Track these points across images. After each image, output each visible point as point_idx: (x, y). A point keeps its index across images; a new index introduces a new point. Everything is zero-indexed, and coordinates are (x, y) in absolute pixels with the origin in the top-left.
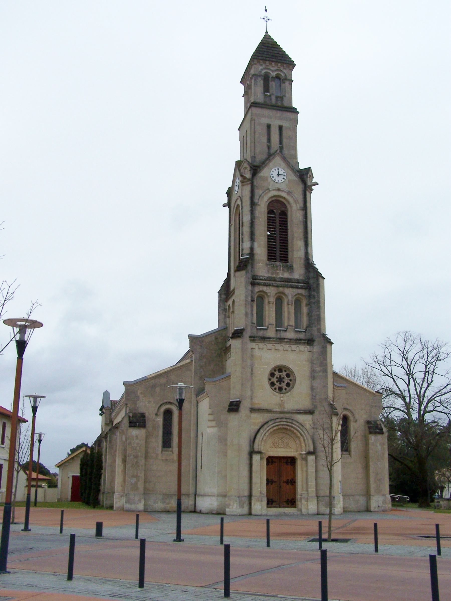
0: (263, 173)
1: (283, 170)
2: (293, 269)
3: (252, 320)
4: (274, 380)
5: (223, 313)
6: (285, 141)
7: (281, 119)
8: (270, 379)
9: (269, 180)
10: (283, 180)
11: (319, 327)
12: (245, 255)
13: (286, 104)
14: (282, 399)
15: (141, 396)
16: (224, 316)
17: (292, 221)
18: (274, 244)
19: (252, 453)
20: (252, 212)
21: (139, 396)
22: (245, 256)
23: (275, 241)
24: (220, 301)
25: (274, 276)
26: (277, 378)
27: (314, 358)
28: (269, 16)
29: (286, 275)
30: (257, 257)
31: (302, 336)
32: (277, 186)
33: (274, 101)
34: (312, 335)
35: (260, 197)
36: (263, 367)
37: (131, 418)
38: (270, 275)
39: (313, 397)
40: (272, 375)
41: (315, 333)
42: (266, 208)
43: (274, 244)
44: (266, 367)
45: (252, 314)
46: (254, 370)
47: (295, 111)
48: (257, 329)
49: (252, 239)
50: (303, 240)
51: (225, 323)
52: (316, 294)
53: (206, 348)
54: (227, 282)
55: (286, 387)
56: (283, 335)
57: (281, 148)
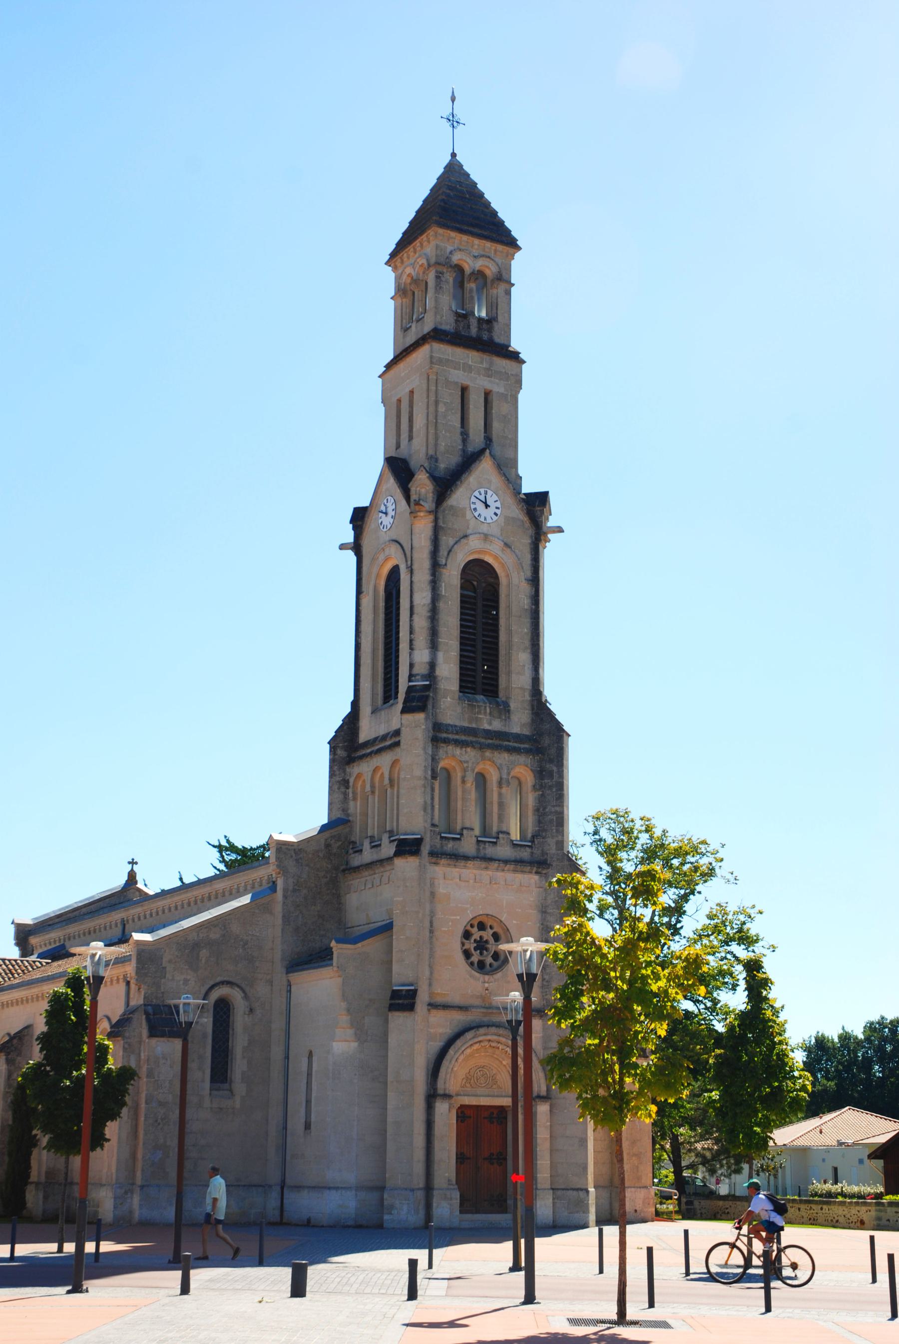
0: (458, 497)
1: (494, 495)
2: (509, 714)
3: (432, 819)
4: (471, 945)
5: (339, 789)
6: (496, 425)
7: (489, 372)
8: (463, 944)
9: (469, 515)
10: (495, 518)
11: (560, 838)
12: (418, 677)
13: (498, 339)
14: (486, 985)
15: (170, 968)
16: (342, 796)
17: (508, 607)
18: (471, 655)
19: (432, 1097)
20: (434, 584)
21: (165, 968)
22: (418, 681)
23: (473, 649)
24: (333, 762)
25: (474, 726)
26: (475, 941)
27: (549, 902)
28: (460, 115)
29: (497, 725)
30: (442, 685)
31: (525, 854)
32: (484, 529)
33: (474, 331)
34: (544, 853)
35: (450, 551)
36: (452, 917)
37: (152, 1017)
38: (466, 724)
39: (545, 983)
40: (467, 935)
41: (552, 849)
42: (459, 577)
43: (471, 655)
44: (458, 918)
45: (433, 807)
46: (434, 924)
47: (515, 357)
48: (442, 838)
49: (434, 645)
50: (529, 651)
51: (345, 810)
52: (555, 769)
53: (307, 865)
54: (351, 722)
55: (492, 961)
56: (490, 851)
57: (488, 440)
